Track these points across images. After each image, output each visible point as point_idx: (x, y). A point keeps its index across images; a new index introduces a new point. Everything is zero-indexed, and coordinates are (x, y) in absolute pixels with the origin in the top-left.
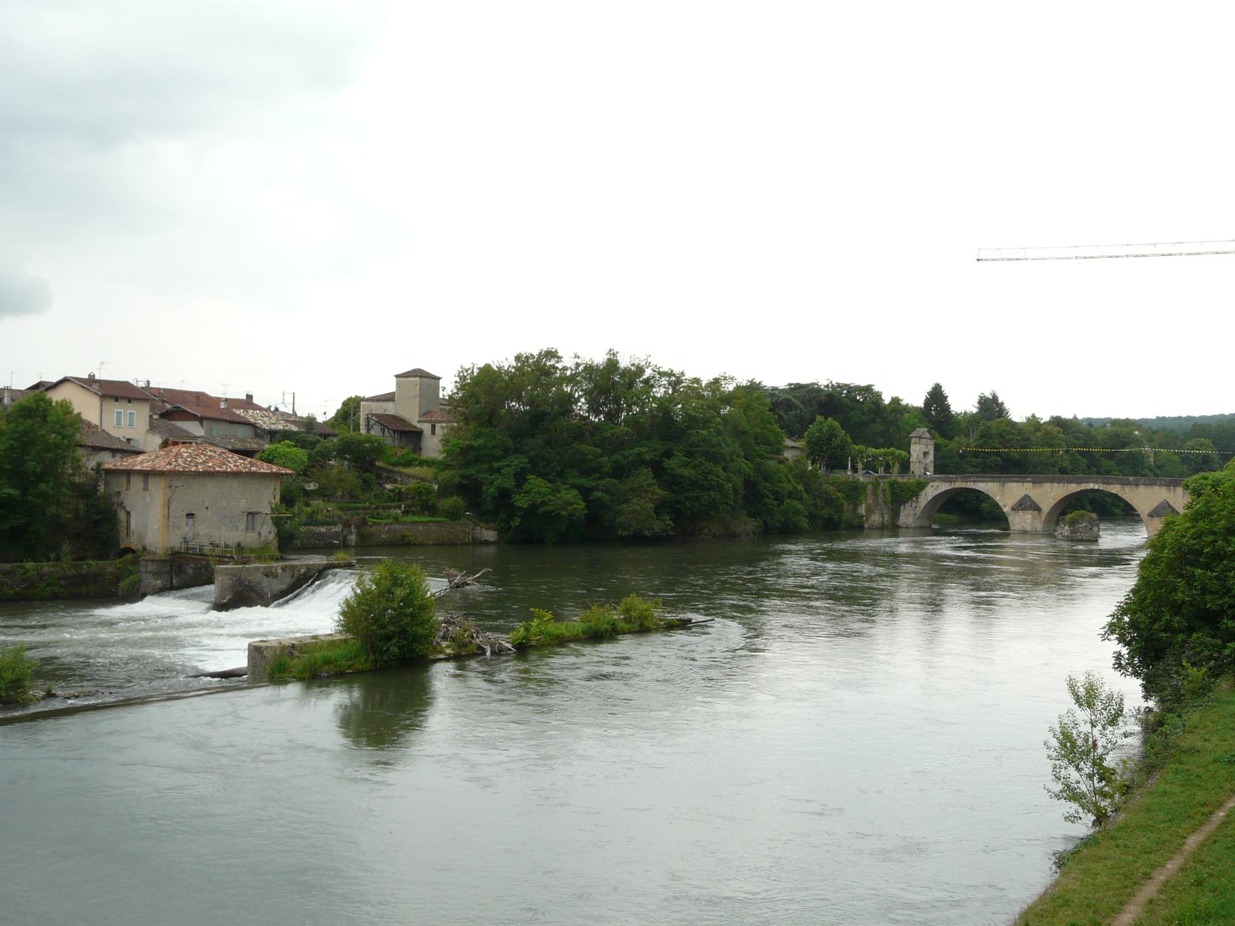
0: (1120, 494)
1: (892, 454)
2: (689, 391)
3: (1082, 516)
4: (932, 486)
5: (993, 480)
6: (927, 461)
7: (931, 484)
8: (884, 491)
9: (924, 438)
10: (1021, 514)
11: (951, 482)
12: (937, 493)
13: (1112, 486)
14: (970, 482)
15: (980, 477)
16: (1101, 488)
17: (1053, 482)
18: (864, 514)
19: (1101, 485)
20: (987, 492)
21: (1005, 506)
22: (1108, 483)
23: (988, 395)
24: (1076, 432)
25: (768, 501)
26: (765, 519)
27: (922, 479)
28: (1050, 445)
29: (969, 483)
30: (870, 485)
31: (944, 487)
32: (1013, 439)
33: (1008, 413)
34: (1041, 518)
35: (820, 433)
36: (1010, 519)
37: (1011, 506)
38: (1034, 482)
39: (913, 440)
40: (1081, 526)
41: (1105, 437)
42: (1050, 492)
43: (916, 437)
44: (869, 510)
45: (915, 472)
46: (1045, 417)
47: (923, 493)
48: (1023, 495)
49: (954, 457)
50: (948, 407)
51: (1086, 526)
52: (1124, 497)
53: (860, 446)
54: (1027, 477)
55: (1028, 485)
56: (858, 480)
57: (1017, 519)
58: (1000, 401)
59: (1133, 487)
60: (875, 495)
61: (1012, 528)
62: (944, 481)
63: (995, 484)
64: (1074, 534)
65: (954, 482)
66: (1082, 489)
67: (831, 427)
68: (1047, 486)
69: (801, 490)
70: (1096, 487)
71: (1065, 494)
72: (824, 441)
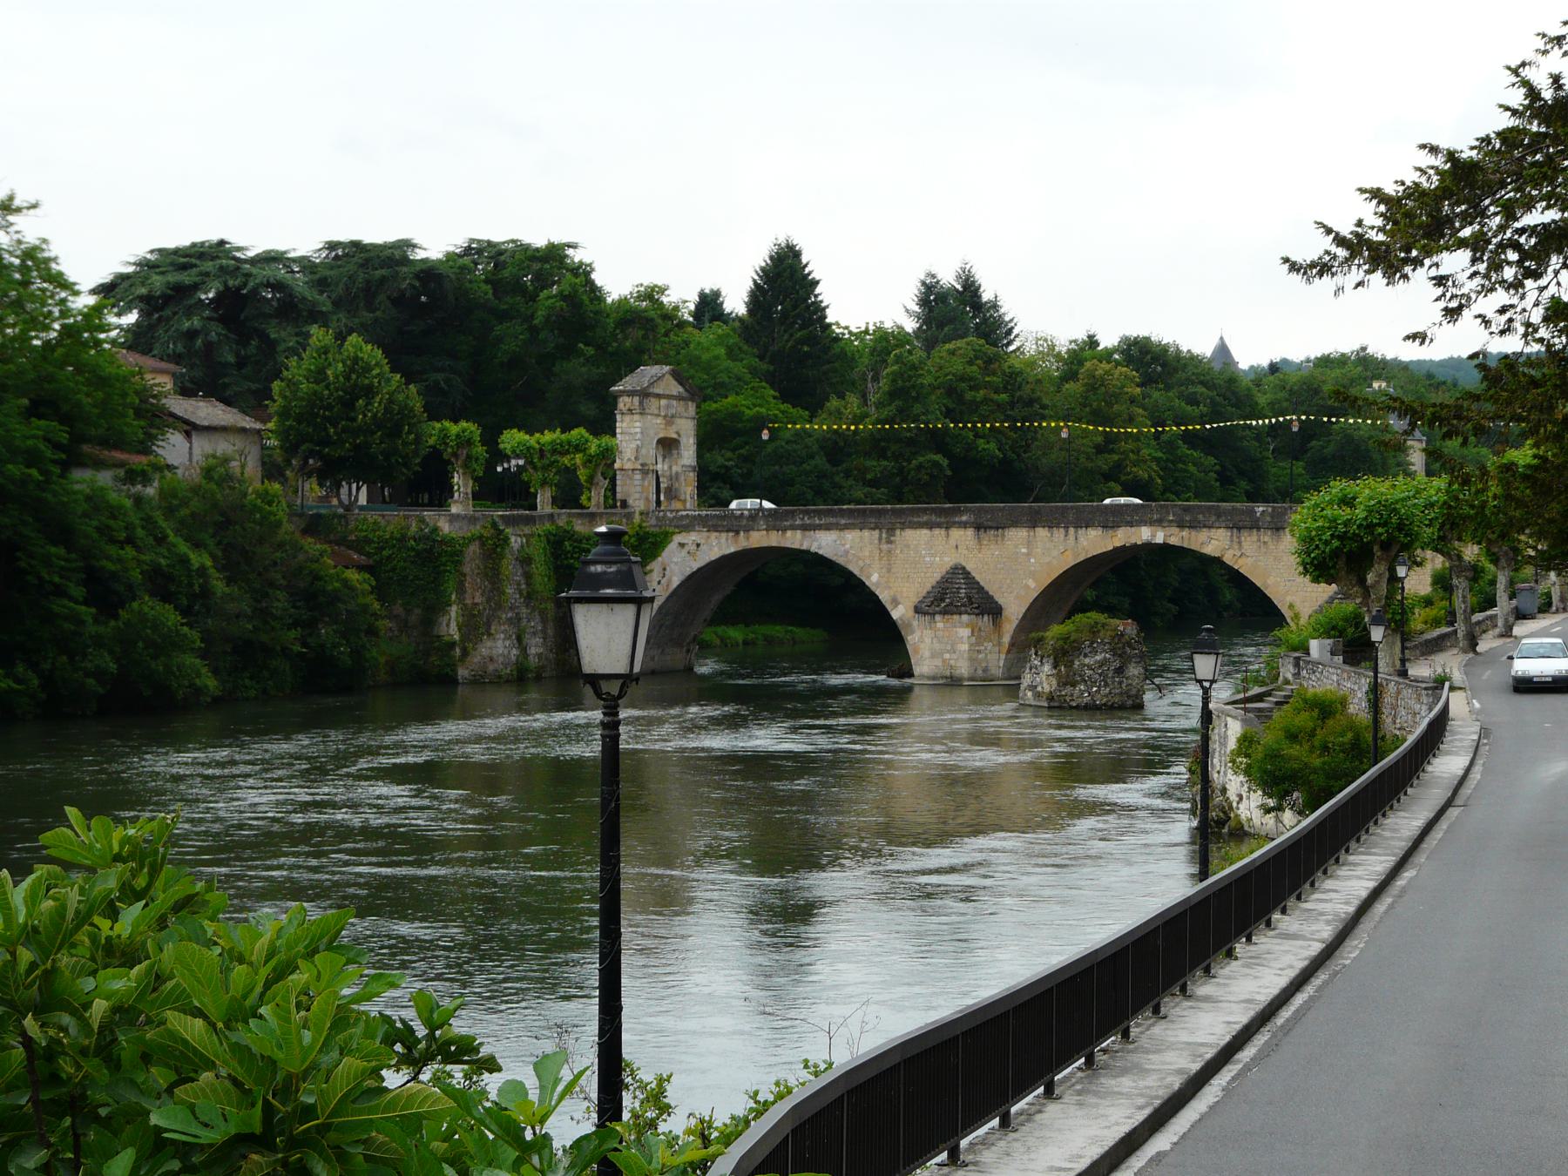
0: (1228, 559)
1: (579, 448)
2: (1303, 417)
3: (1094, 630)
4: (682, 545)
5: (860, 520)
6: (675, 469)
7: (678, 539)
8: (526, 561)
9: (659, 396)
10: (940, 625)
11: (737, 533)
12: (696, 566)
13: (1203, 535)
14: (793, 528)
15: (819, 513)
16: (1173, 541)
17: (1033, 525)
18: (457, 637)
19: (1175, 530)
20: (841, 561)
21: (896, 602)
22: (1194, 525)
23: (948, 278)
24: (1189, 382)
25: (59, 606)
26: (46, 666)
27: (651, 524)
28: (1098, 417)
29: (789, 533)
30: (474, 548)
31: (718, 546)
32: (986, 400)
33: (1011, 330)
34: (1000, 636)
35: (317, 382)
36: (912, 640)
37: (914, 600)
38: (979, 527)
39: (624, 403)
40: (1087, 661)
41: (1281, 395)
42: (1028, 555)
43: (631, 393)
44: (475, 628)
45: (630, 502)
46: (1108, 340)
47: (655, 566)
48: (947, 567)
49: (812, 457)
50: (819, 310)
51: (1102, 664)
52: (1245, 566)
53: (464, 424)
54: (959, 512)
55: (963, 537)
56: (436, 530)
57: (928, 640)
58: (986, 296)
59: (1267, 537)
60: (493, 575)
61: (917, 670)
62: (715, 528)
63: (866, 533)
64: (1069, 689)
65: (747, 530)
66: (1118, 544)
67: (356, 365)
68: (1017, 536)
69: (202, 570)
70: (1159, 538)
71: (1070, 561)
72: (329, 407)
